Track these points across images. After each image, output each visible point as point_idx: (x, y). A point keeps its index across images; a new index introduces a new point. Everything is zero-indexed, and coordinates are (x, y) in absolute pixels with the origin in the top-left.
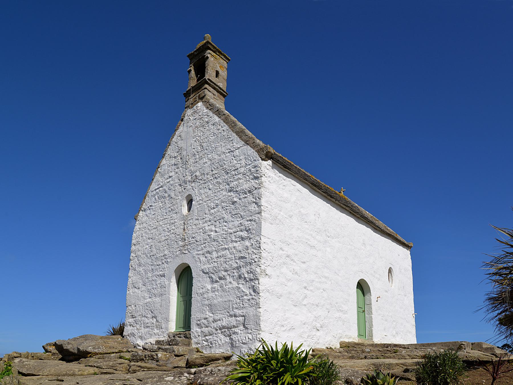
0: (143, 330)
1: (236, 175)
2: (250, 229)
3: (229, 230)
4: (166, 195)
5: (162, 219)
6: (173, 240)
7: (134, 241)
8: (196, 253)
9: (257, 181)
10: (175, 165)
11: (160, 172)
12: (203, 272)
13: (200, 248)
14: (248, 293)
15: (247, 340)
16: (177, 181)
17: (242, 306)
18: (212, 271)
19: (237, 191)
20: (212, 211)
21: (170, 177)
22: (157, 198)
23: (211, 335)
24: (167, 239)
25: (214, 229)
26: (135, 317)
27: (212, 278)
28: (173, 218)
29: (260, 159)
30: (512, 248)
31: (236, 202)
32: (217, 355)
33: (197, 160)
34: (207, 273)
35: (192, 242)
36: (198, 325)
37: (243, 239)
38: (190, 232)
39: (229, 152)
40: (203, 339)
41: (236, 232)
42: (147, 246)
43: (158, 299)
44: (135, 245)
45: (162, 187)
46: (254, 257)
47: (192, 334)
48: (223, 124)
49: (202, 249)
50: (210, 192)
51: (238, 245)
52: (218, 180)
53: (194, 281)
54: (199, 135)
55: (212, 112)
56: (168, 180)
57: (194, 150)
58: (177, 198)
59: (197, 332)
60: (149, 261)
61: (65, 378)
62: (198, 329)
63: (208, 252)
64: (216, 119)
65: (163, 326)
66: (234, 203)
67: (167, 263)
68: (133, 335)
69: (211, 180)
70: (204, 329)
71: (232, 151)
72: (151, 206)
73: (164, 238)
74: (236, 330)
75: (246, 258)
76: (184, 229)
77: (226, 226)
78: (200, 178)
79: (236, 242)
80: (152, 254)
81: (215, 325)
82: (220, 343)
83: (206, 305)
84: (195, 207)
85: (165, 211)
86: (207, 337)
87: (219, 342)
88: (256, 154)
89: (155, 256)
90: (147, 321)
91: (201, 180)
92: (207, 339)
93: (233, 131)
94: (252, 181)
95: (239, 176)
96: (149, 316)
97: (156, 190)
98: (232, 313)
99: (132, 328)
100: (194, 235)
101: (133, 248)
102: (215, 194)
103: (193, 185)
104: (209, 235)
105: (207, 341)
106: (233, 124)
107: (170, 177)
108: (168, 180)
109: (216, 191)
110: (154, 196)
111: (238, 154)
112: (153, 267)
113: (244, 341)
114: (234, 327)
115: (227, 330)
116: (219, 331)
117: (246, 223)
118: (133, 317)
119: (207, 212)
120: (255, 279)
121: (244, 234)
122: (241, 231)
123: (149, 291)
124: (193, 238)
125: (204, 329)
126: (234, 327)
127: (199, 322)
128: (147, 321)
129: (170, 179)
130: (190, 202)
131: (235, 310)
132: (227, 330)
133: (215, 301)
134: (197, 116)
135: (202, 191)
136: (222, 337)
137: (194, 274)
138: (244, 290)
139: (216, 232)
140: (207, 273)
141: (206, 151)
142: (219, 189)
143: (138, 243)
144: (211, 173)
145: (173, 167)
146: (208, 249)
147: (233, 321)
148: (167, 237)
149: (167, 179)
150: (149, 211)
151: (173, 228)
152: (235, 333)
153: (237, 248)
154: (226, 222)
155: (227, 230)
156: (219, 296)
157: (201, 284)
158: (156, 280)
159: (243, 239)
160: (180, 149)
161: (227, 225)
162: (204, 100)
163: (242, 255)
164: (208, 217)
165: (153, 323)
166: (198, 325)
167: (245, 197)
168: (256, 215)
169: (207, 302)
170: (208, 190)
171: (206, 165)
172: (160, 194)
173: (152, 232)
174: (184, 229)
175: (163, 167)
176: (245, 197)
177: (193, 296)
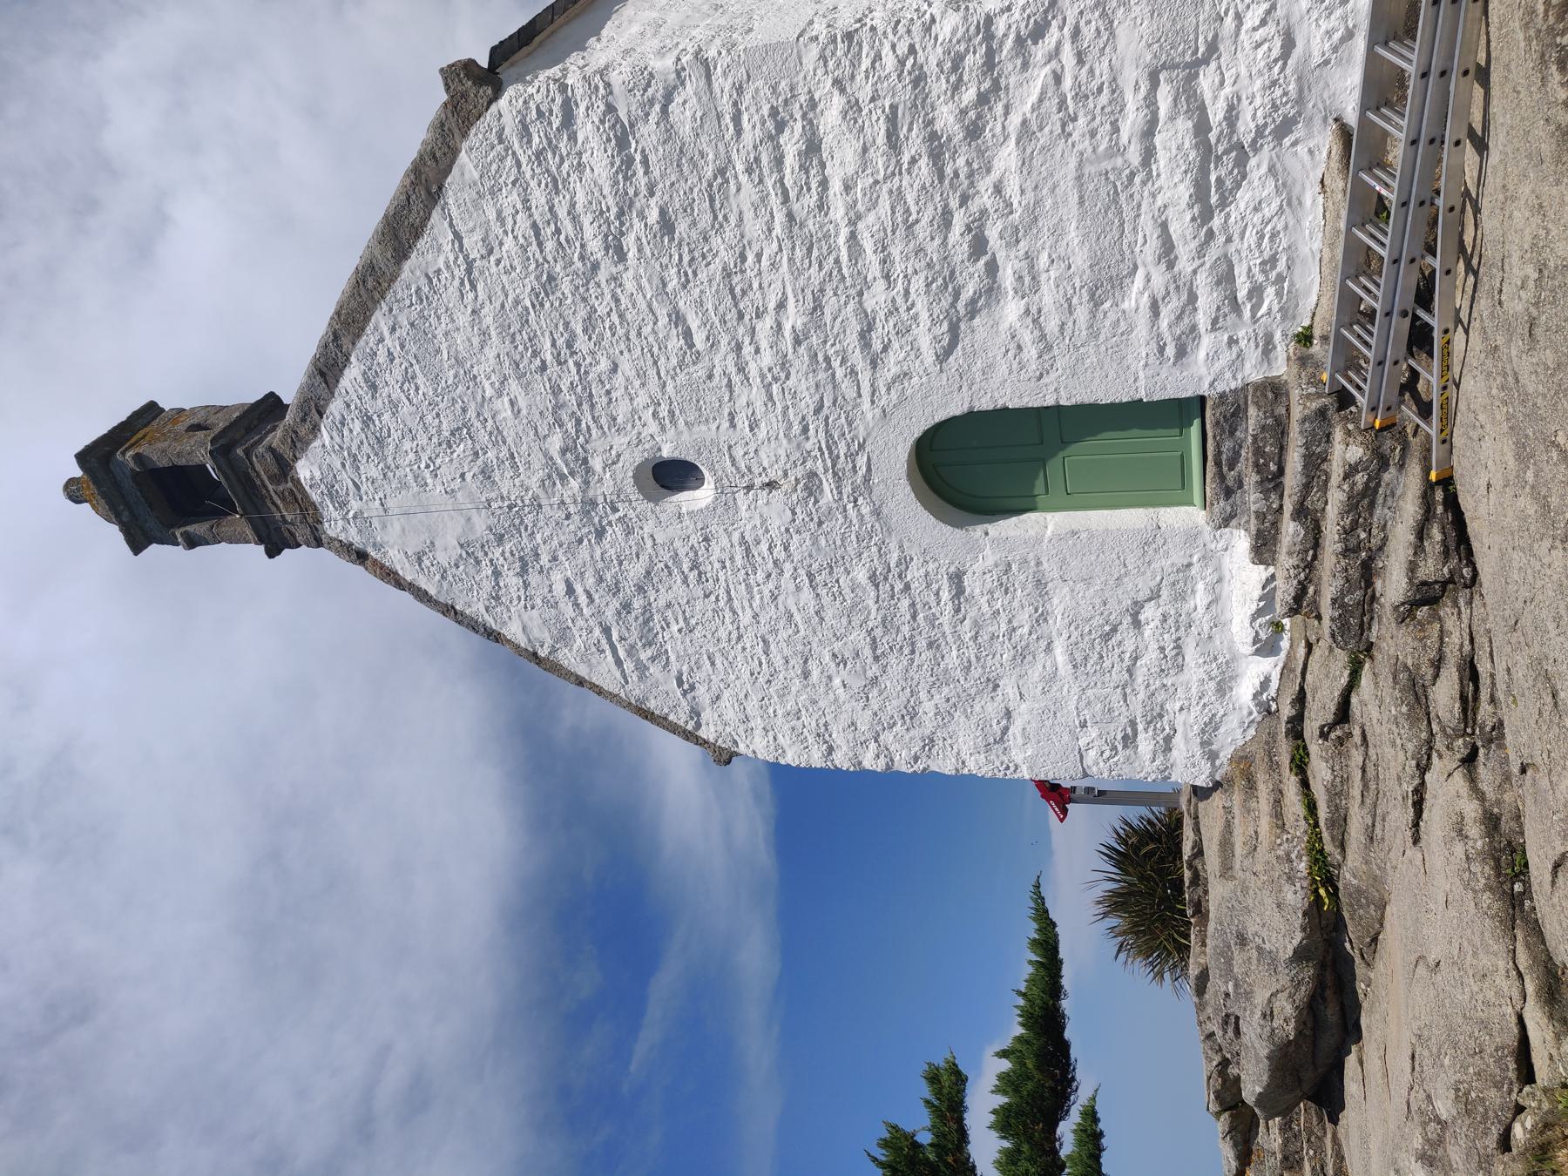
0: (1194, 670)
1: (558, 231)
2: (774, 112)
3: (778, 230)
4: (637, 604)
5: (728, 614)
6: (815, 542)
7: (816, 759)
8: (866, 405)
9: (582, 109)
10: (524, 571)
11: (554, 650)
12: (949, 351)
13: (847, 389)
14: (1047, 69)
15: (1270, 29)
16: (584, 552)
17: (1104, 98)
18: (945, 304)
19: (621, 214)
20: (699, 339)
21: (570, 591)
22: (649, 653)
23: (1231, 267)
24: (811, 576)
25: (769, 321)
26: (1133, 724)
27: (973, 301)
28: (726, 556)
29: (493, 108)
30: (1060, 3)
31: (663, 212)
32: (1335, 148)
33: (504, 454)
34: (954, 330)
35: (822, 435)
36: (1181, 352)
37: (812, 147)
38: (782, 452)
39: (474, 287)
40: (1247, 313)
41: (785, 193)
42: (837, 682)
43: (1059, 602)
44: (831, 750)
45: (607, 631)
46: (889, 61)
47: (1221, 387)
48: (368, 340)
49: (853, 372)
50: (626, 366)
51: (841, 159)
52: (579, 331)
53: (985, 404)
54: (411, 456)
55: (327, 402)
56: (583, 599)
57: (468, 477)
58: (649, 543)
59: (1212, 358)
60: (896, 664)
61: (1447, 446)
62: (1202, 354)
63: (865, 336)
64: (352, 375)
65: (1178, 558)
66: (667, 225)
67: (904, 562)
68: (1211, 726)
69: (578, 365)
70: (1203, 320)
71: (469, 271)
72: (680, 683)
73: (807, 595)
74: (1216, 114)
75: (894, 108)
76: (771, 485)
77: (759, 256)
78: (570, 426)
79: (824, 184)
80: (867, 652)
81: (1184, 253)
82: (1275, 205)
83: (1093, 314)
84: (686, 436)
85: (699, 605)
86: (1242, 294)
87: (1267, 212)
88: (475, 137)
89: (878, 632)
90: (1150, 657)
91: (578, 422)
92: (1250, 296)
93: (393, 280)
94: (580, 138)
95: (562, 212)
96: (1129, 646)
97: (619, 663)
98: (1134, 156)
99: (1178, 740)
100: (796, 428)
101: (841, 760)
102: (633, 335)
103: (596, 463)
104: (797, 342)
105: (1256, 292)
106: (370, 285)
107: (570, 591)
108: (583, 599)
109: (620, 332)
110: (641, 668)
111: (477, 236)
112: (922, 643)
113: (1276, 52)
114: (1202, 128)
115: (1218, 162)
116: (1216, 222)
117: (748, 137)
118: (1129, 740)
119: (699, 372)
120: (989, 37)
121: (791, 144)
122: (779, 161)
123: (1022, 655)
124: (805, 430)
125: (1203, 320)
126: (1202, 128)
127: (1170, 351)
128: (1150, 657)
129: (579, 589)
130: (671, 475)
131: (1124, 139)
132: (1218, 162)
133: (1080, 260)
134: (345, 478)
135: (622, 410)
136: (1244, 197)
137: (956, 408)
138: (1033, 98)
139: (781, 306)
140: (954, 330)
141: (471, 413)
142: (615, 317)
143: (822, 735)
144: (553, 369)
145: (534, 578)
146: (852, 339)
147: (1174, 137)
148: (802, 572)
149: (576, 605)
150: (701, 690)
151: (764, 547)
152: (1231, 116)
153: (850, 170)
154: (743, 258)
155: (775, 245)
156: (1054, 247)
157: (1006, 373)
158: (975, 623)
159: (812, 147)
160: (470, 552)
161: (756, 248)
162: (288, 455)
163: (881, 140)
164: (723, 360)
165: (1165, 618)
166: (1181, 352)
167: (645, 162)
168: (716, 86)
169: (1082, 313)
170: (619, 380)
171: (522, 403)
172: (634, 636)
173: (779, 662)
174: (771, 485)
175: (536, 633)
176: (645, 162)
177: (1050, 401)
